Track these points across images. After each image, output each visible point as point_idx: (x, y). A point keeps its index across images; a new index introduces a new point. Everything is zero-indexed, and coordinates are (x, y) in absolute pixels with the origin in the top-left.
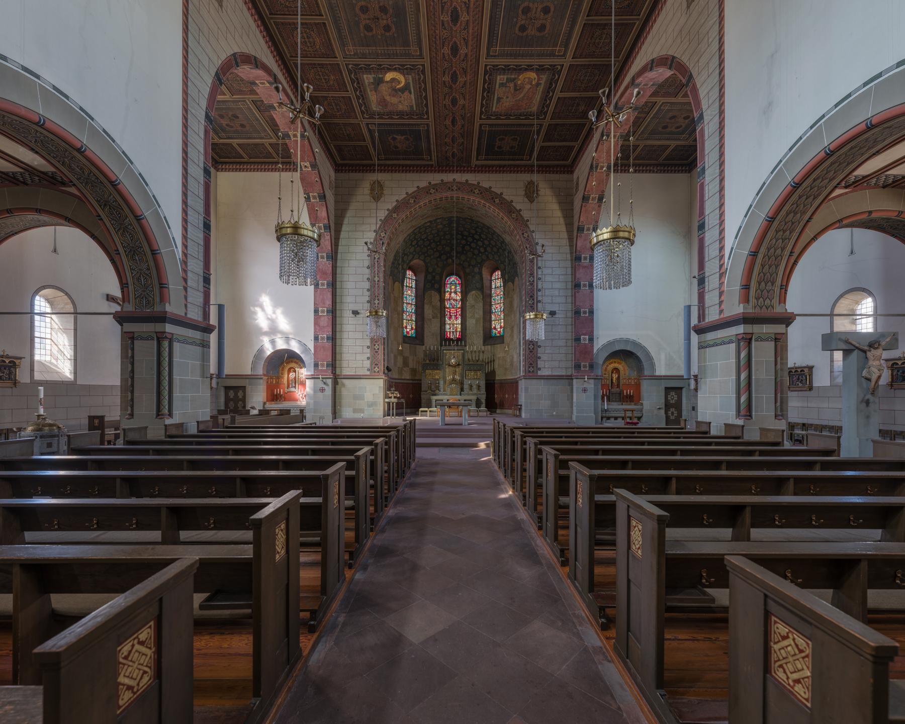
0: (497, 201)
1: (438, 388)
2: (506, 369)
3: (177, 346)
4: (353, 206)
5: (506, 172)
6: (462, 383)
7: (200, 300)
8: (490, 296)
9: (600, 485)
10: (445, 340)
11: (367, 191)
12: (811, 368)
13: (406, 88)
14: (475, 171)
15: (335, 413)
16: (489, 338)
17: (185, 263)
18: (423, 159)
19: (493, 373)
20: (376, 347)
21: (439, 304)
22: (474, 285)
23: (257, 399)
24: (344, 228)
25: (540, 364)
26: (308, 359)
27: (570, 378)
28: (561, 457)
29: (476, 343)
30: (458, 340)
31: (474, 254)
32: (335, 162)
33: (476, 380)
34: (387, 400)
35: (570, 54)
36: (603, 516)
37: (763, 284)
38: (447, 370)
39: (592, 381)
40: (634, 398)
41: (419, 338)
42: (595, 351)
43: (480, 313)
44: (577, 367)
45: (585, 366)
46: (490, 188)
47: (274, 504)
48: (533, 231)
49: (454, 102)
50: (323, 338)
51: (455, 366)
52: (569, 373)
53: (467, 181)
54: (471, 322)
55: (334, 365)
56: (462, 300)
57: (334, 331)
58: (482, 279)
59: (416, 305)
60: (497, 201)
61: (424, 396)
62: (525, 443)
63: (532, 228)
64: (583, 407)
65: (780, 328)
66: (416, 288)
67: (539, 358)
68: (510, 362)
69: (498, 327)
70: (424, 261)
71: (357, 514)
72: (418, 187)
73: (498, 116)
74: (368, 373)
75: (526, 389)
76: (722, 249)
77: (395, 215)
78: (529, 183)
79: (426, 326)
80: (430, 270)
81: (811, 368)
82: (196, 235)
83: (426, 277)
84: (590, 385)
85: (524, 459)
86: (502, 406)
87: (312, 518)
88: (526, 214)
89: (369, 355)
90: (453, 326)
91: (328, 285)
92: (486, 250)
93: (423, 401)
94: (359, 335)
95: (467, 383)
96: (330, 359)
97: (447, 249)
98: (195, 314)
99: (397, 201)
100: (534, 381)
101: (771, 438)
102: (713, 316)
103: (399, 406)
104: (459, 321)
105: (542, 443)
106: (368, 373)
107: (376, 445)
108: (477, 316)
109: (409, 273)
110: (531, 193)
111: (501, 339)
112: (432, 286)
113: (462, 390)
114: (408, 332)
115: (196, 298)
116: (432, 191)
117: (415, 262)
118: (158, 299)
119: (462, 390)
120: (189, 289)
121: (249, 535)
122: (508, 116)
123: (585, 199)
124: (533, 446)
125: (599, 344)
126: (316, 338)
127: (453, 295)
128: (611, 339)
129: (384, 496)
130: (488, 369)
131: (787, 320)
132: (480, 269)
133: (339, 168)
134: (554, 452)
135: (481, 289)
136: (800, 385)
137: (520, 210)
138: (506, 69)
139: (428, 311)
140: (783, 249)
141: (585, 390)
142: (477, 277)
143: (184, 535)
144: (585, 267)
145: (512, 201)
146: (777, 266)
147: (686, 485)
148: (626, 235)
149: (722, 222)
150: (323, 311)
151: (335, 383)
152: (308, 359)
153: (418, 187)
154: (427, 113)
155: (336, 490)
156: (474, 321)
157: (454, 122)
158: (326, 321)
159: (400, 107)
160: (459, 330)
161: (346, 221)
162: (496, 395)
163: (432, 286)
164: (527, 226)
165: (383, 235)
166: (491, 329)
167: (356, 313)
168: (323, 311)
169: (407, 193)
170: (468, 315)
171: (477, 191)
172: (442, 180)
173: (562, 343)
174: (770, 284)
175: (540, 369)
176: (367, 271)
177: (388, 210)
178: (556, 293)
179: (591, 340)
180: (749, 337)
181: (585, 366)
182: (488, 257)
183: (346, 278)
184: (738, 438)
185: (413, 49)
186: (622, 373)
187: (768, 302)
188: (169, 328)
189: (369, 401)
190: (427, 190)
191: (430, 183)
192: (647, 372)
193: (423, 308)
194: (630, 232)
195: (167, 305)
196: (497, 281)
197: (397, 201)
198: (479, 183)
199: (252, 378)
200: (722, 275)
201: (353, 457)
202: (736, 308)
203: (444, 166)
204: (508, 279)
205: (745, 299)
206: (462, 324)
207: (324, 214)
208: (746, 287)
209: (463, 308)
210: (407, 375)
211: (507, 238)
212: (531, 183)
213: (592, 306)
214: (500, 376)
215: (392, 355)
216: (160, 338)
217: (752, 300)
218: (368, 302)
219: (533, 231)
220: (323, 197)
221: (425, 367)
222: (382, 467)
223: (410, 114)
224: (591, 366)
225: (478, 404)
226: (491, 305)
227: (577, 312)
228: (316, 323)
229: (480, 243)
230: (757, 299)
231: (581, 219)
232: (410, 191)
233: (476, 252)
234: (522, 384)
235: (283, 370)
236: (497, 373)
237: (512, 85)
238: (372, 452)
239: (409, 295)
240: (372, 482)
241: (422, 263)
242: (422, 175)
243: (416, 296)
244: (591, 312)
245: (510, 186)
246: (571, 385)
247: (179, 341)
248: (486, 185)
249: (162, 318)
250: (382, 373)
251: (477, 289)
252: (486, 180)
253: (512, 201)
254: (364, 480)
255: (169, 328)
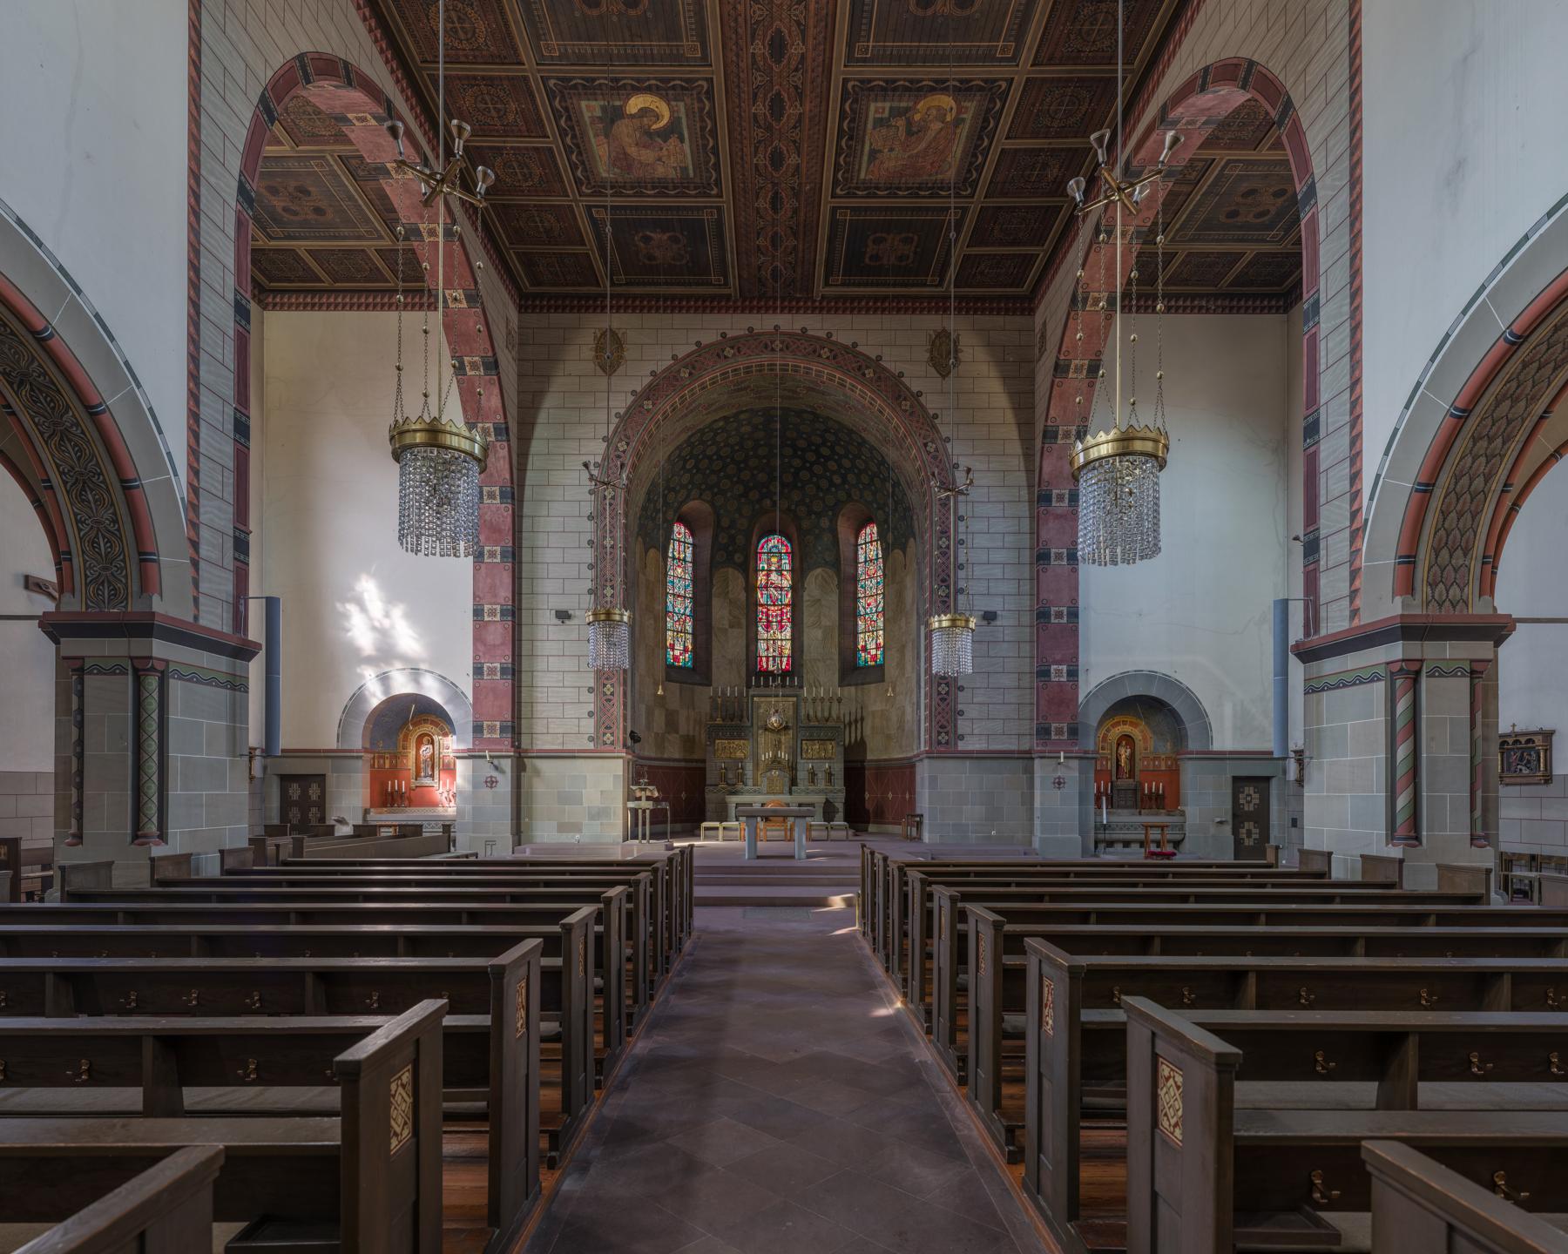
0: (869, 373)
1: (741, 778)
2: (889, 737)
3: (176, 687)
4: (558, 384)
5: (890, 310)
6: (793, 768)
7: (227, 587)
8: (855, 579)
9: (1092, 987)
10: (757, 675)
11: (588, 353)
12: (1548, 735)
13: (672, 129)
14: (821, 310)
15: (519, 832)
16: (852, 670)
17: (193, 507)
18: (710, 284)
19: (861, 745)
20: (609, 689)
21: (743, 596)
22: (819, 556)
23: (350, 802)
24: (539, 431)
25: (963, 726)
26: (460, 715)
27: (1027, 757)
28: (1008, 928)
29: (823, 680)
30: (785, 674)
31: (818, 488)
32: (519, 289)
33: (826, 761)
34: (631, 805)
35: (1027, 56)
36: (1099, 1055)
37: (1445, 553)
38: (762, 740)
39: (1075, 764)
40: (1165, 800)
41: (700, 670)
42: (1081, 699)
43: (832, 616)
44: (1043, 732)
45: (1059, 731)
46: (855, 345)
47: (387, 1029)
48: (948, 440)
49: (777, 159)
50: (492, 671)
51: (777, 731)
52: (1026, 747)
53: (804, 330)
54: (812, 636)
55: (515, 728)
56: (792, 587)
57: (517, 655)
58: (836, 541)
59: (694, 599)
60: (869, 373)
61: (710, 796)
62: (930, 897)
63: (945, 431)
64: (1055, 818)
65: (1481, 649)
66: (694, 562)
67: (961, 713)
68: (898, 722)
69: (871, 645)
70: (712, 504)
71: (567, 1052)
72: (698, 344)
73: (871, 189)
74: (591, 746)
75: (933, 780)
76: (1355, 477)
77: (648, 405)
78: (938, 335)
79: (715, 644)
80: (725, 522)
81: (1548, 735)
82: (219, 446)
83: (715, 537)
84: (1072, 772)
85: (928, 932)
86: (880, 817)
87: (469, 1060)
88: (931, 403)
89: (591, 707)
90: (775, 644)
91: (503, 555)
92: (845, 481)
93: (710, 807)
94: (571, 664)
95: (804, 767)
96: (508, 716)
97: (762, 477)
98: (215, 619)
99: (653, 373)
100: (950, 764)
101: (1463, 888)
102: (1335, 622)
103: (657, 817)
104: (787, 633)
105: (966, 897)
106: (591, 746)
107: (608, 901)
108: (825, 622)
109: (679, 530)
110: (943, 356)
111: (877, 673)
112: (728, 558)
113: (794, 782)
114: (676, 658)
115: (217, 582)
116: (729, 352)
117: (693, 505)
118: (135, 586)
119: (794, 782)
120: (202, 564)
121: (332, 1096)
122: (892, 190)
123: (1060, 369)
124: (946, 904)
125: (1089, 683)
126: (478, 671)
127: (774, 577)
128: (1116, 671)
129: (624, 1011)
130: (850, 737)
131: (1498, 630)
132: (833, 521)
133: (526, 303)
134: (992, 917)
135: (836, 565)
136: (1526, 771)
137: (920, 394)
138: (889, 88)
139: (720, 613)
140: (1488, 478)
141: (1059, 783)
142: (827, 538)
143: (192, 1096)
144: (1058, 517)
145: (901, 375)
146: (1475, 515)
147: (1277, 988)
148: (1148, 446)
149: (1356, 420)
150: (492, 613)
151: (520, 767)
152: (460, 715)
153: (698, 344)
154: (718, 183)
155: (521, 999)
156: (819, 634)
157: (775, 202)
158: (498, 632)
159: (660, 171)
160: (787, 652)
161: (542, 417)
162: (867, 794)
163: (728, 558)
164: (934, 427)
165: (622, 446)
166: (855, 650)
167: (563, 616)
168: (492, 613)
169: (674, 357)
170: (807, 620)
171: (825, 353)
172: (751, 329)
173: (1009, 681)
174: (1459, 552)
175: (962, 737)
176: (589, 526)
177: (634, 392)
178: (997, 572)
179: (1073, 674)
180: (1414, 667)
181: (1059, 731)
182: (849, 495)
183: (541, 540)
184: (1321, 875)
185: (688, 45)
186: (1139, 745)
187: (1454, 592)
188: (160, 649)
189: (592, 807)
190: (717, 351)
191: (724, 335)
192: (1192, 745)
193: (709, 603)
194: (1156, 441)
195: (156, 598)
196: (869, 547)
197: (653, 373)
198: (829, 335)
199: (339, 756)
200: (1355, 534)
201: (557, 929)
202: (1386, 606)
203: (755, 298)
204: (894, 543)
205: (1407, 586)
206: (793, 639)
207: (495, 402)
208: (1408, 560)
209: (796, 605)
210: (674, 751)
211: (892, 455)
212: (943, 335)
213: (1075, 600)
214: (875, 752)
215: (643, 707)
216: (140, 669)
217: (1422, 588)
218: (590, 592)
219: (948, 440)
220: (492, 365)
221: (714, 732)
222: (607, 955)
223: (681, 186)
224: (1074, 732)
225: (829, 814)
226: (856, 599)
227: (1042, 615)
228: (478, 638)
229: (832, 465)
230: (1432, 585)
231: (1052, 413)
232: (682, 352)
233: (824, 484)
234: (924, 770)
235: (406, 739)
236: (870, 744)
237: (901, 123)
238: (600, 917)
239: (680, 578)
240: (598, 981)
241: (706, 507)
242: (707, 317)
243: (695, 580)
244: (1074, 614)
245: (895, 341)
246: (1030, 772)
247: (181, 677)
248: (844, 338)
249: (145, 627)
250: (619, 746)
251: (826, 564)
252: (846, 329)
253: (901, 375)
254: (581, 979)
255: (160, 649)
